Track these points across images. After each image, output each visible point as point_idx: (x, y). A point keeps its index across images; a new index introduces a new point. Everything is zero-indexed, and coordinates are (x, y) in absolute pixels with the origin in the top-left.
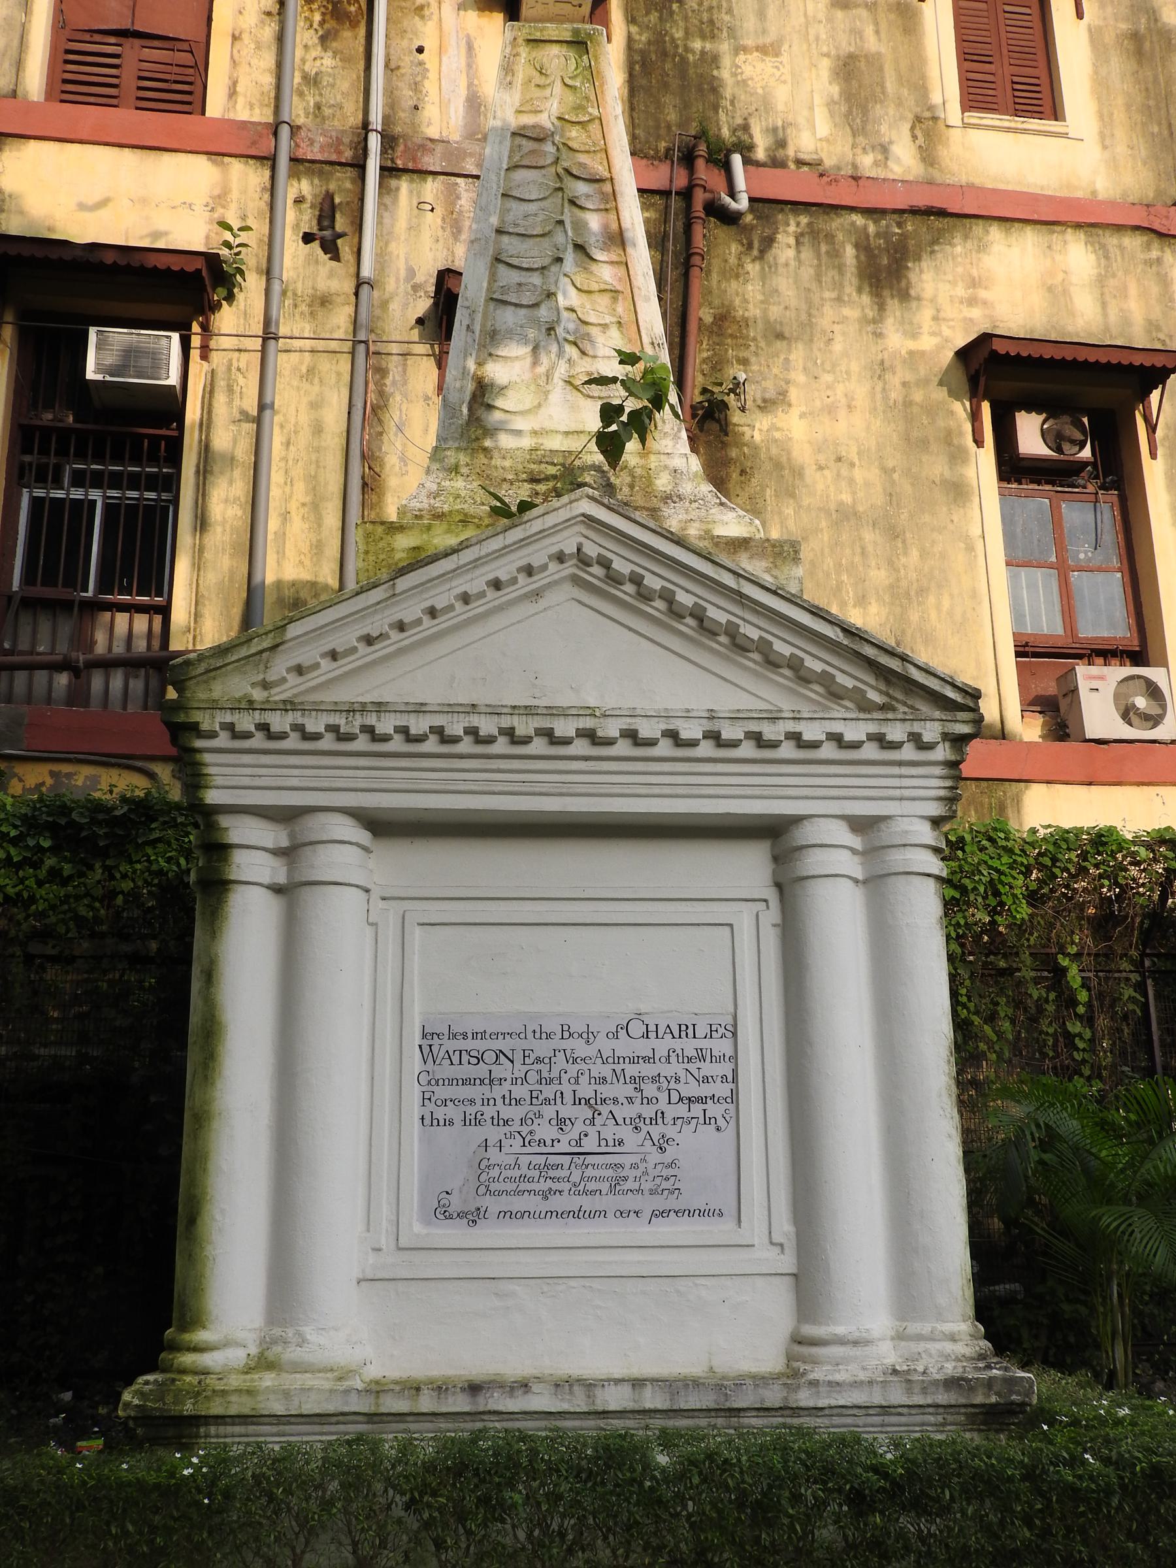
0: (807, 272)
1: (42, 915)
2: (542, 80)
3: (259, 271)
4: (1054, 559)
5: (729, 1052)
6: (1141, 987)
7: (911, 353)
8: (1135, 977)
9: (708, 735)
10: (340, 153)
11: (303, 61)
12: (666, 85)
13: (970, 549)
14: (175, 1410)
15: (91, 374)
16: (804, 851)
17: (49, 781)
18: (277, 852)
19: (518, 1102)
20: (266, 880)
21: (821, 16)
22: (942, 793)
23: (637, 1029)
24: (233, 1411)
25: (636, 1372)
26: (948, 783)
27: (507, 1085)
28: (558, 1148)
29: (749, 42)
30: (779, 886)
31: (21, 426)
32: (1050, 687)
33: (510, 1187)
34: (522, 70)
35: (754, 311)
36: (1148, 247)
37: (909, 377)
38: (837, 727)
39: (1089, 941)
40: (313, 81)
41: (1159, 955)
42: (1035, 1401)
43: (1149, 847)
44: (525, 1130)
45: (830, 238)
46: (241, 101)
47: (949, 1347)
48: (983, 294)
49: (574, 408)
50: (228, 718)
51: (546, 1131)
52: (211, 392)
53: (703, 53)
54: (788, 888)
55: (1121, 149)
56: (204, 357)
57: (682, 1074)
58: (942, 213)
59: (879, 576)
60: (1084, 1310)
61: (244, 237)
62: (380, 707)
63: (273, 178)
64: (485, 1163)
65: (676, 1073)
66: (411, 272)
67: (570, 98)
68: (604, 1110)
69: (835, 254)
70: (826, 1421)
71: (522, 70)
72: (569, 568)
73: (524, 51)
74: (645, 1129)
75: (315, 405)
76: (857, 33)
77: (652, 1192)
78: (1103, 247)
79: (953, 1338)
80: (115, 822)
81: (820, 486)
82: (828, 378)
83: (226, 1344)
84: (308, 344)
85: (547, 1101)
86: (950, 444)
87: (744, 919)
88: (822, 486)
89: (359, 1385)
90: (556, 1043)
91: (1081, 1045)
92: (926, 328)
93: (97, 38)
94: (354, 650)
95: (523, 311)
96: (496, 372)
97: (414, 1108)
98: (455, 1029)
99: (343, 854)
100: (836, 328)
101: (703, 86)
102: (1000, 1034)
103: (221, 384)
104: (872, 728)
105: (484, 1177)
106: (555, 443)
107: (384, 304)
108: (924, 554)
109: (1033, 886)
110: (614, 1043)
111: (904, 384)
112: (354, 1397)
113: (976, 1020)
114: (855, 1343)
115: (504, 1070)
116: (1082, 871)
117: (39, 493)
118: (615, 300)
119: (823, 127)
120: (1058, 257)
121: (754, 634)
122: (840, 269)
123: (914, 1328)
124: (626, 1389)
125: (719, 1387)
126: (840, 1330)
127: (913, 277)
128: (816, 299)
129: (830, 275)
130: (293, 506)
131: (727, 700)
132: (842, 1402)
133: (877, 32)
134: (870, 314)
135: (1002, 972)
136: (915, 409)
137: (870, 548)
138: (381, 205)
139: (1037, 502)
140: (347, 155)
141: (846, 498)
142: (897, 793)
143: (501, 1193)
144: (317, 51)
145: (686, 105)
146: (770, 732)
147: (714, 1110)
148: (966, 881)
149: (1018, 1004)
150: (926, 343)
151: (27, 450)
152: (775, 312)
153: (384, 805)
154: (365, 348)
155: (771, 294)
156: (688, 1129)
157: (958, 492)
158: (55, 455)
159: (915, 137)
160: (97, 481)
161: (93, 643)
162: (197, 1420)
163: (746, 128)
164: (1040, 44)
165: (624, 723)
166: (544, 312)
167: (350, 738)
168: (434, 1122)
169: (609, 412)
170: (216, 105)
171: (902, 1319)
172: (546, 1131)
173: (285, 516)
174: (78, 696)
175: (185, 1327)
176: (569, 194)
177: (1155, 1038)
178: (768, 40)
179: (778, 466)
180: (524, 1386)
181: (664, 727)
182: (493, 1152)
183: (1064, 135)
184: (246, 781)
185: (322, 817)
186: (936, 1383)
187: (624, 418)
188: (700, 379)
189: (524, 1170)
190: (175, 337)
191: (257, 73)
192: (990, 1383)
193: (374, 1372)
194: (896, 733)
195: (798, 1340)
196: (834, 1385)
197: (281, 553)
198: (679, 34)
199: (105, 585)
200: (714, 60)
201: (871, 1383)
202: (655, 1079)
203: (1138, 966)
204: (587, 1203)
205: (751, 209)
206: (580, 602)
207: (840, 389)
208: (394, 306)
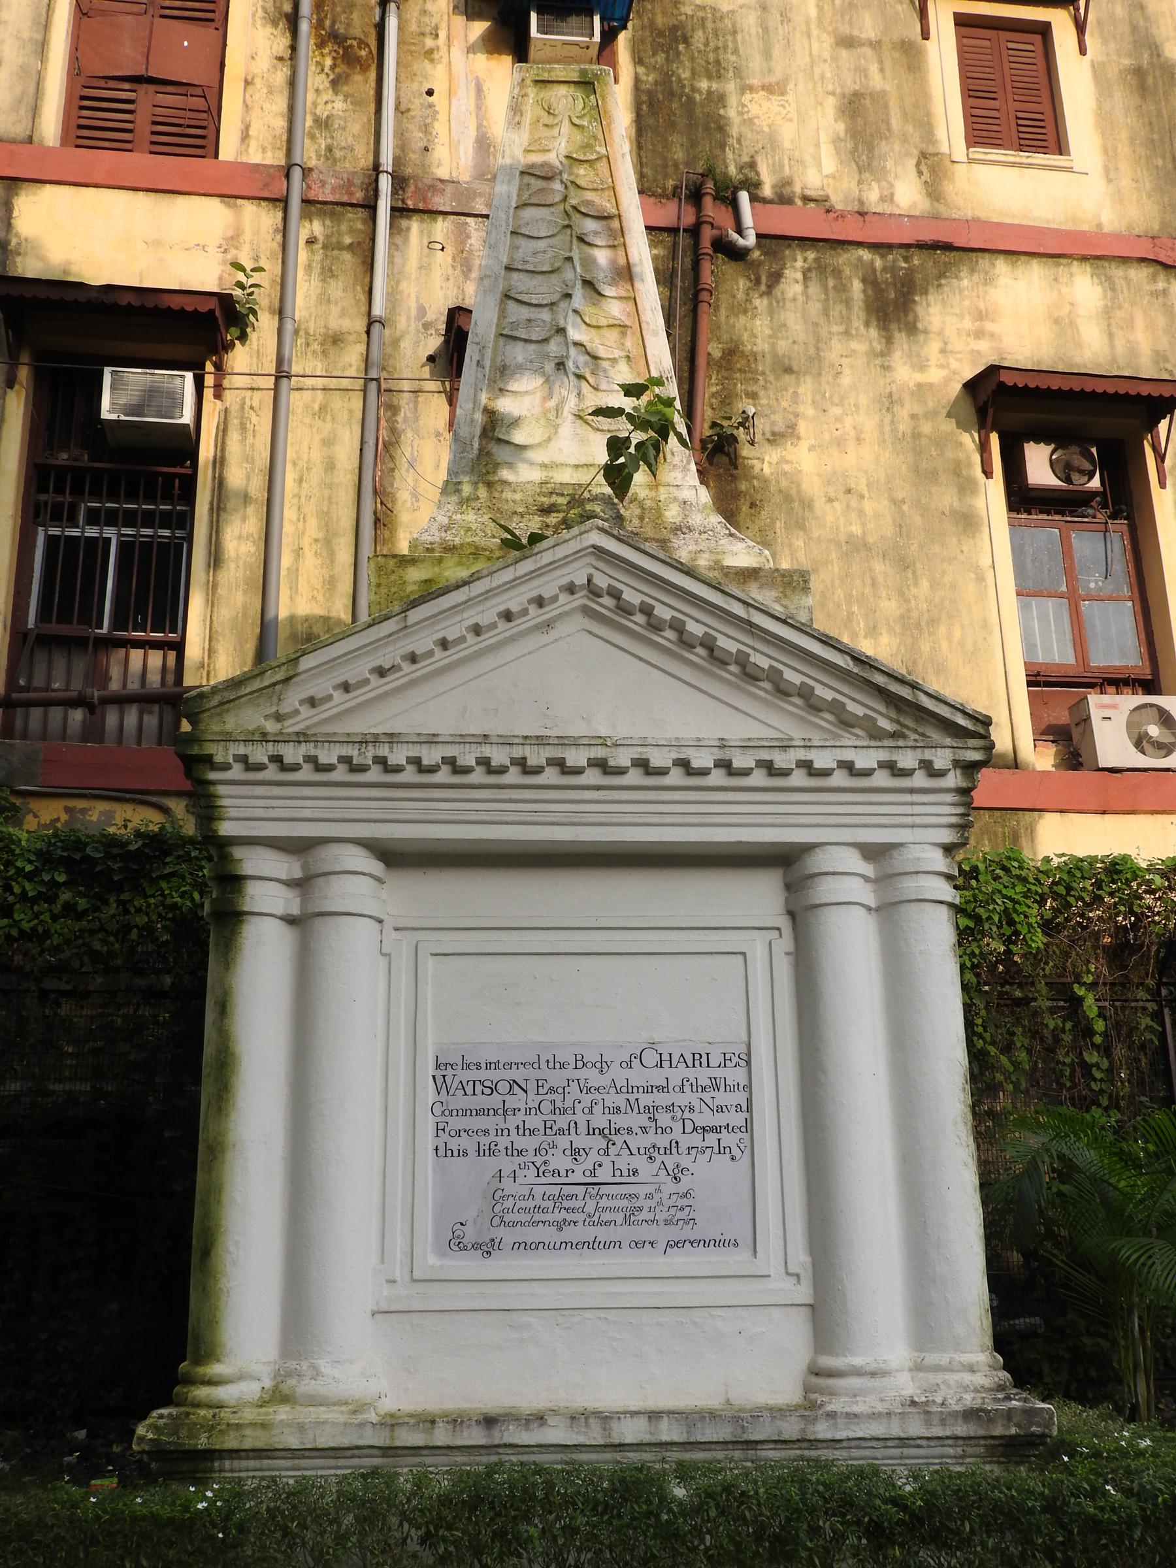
0: (815, 307)
2: (549, 120)
3: (271, 311)
4: (1064, 589)
6: (1158, 1016)
7: (919, 385)
8: (1152, 1006)
10: (351, 194)
11: (315, 105)
12: (673, 125)
13: (980, 579)
14: (189, 1444)
17: (64, 817)
18: (290, 884)
20: (280, 911)
21: (826, 55)
22: (954, 820)
23: (650, 1058)
24: (247, 1445)
25: (652, 1404)
27: (520, 1116)
29: (755, 82)
30: (791, 914)
31: (36, 465)
32: (1061, 716)
33: (527, 1217)
34: (530, 110)
35: (762, 346)
36: (1154, 278)
37: (918, 409)
38: (848, 755)
40: (323, 124)
44: (539, 1160)
45: (837, 272)
46: (253, 144)
47: (967, 1378)
48: (989, 326)
49: (583, 441)
51: (560, 1162)
52: (225, 431)
53: (710, 92)
54: (801, 915)
55: (1126, 183)
56: (218, 396)
57: (696, 1103)
58: (948, 247)
59: (889, 606)
61: (256, 278)
62: (392, 739)
63: (285, 219)
64: (499, 1194)
65: (691, 1106)
66: (422, 311)
67: (578, 137)
68: (619, 1139)
69: (842, 289)
70: (845, 1453)
71: (530, 110)
72: (580, 599)
73: (532, 92)
74: (659, 1159)
77: (667, 1223)
78: (1109, 279)
79: (971, 1369)
80: (129, 856)
81: (830, 519)
82: (837, 411)
84: (320, 382)
85: (561, 1131)
88: (831, 517)
89: (374, 1418)
91: (1098, 1075)
93: (112, 84)
94: (366, 682)
95: (533, 347)
98: (468, 1059)
99: (356, 885)
100: (845, 361)
101: (709, 124)
102: (1016, 1065)
103: (234, 422)
104: (884, 755)
105: (498, 1208)
106: (566, 476)
107: (395, 343)
108: (934, 585)
109: (1048, 915)
110: (627, 1073)
111: (913, 417)
112: (368, 1430)
113: (992, 1050)
114: (873, 1374)
115: (517, 1100)
116: (1098, 899)
117: (55, 531)
118: (624, 334)
119: (829, 164)
120: (1065, 290)
121: (764, 663)
122: (848, 303)
123: (932, 1358)
124: (642, 1423)
125: (736, 1419)
126: (857, 1361)
127: (920, 310)
128: (824, 332)
129: (838, 309)
130: (306, 542)
132: (860, 1434)
133: (882, 70)
134: (878, 347)
135: (1018, 1002)
136: (924, 441)
138: (393, 245)
139: (1046, 532)
140: (359, 196)
141: (856, 529)
142: (909, 820)
143: (515, 1224)
144: (328, 95)
145: (693, 144)
147: (728, 1139)
148: (980, 911)
149: (1035, 1034)
150: (934, 375)
152: (783, 346)
154: (376, 386)
157: (968, 522)
159: (920, 173)
160: (111, 519)
163: (752, 165)
165: (635, 753)
167: (363, 769)
168: (448, 1152)
169: (616, 445)
170: (229, 148)
172: (560, 1162)
173: (298, 552)
174: (93, 732)
176: (577, 231)
178: (773, 80)
179: (788, 498)
180: (540, 1418)
181: (675, 756)
182: (507, 1183)
183: (1069, 170)
185: (335, 849)
188: (709, 413)
189: (538, 1201)
190: (189, 376)
191: (270, 116)
193: (388, 1405)
194: (907, 760)
195: (816, 1372)
196: (853, 1417)
197: (294, 588)
198: (685, 75)
199: (119, 621)
200: (721, 99)
201: (889, 1414)
202: (670, 1108)
203: (1155, 995)
204: (603, 1234)
205: (759, 245)
206: (590, 633)
207: (849, 421)
208: (406, 345)
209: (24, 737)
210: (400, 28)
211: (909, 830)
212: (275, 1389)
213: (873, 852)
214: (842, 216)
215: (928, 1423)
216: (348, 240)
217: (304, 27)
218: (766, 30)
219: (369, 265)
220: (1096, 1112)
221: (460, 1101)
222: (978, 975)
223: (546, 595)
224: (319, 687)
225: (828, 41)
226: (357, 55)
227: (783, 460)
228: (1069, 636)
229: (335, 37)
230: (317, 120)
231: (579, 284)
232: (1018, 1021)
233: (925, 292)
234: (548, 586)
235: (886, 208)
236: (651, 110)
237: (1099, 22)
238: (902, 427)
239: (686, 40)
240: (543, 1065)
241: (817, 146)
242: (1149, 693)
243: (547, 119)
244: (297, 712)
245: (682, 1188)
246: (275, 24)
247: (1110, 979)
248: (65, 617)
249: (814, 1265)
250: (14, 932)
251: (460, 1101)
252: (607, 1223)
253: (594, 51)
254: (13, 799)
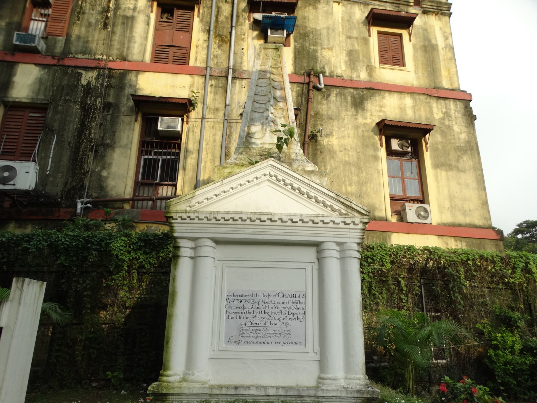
0: (338, 103)
1: (142, 262)
2: (267, 58)
3: (201, 103)
5: (304, 302)
6: (420, 287)
7: (364, 123)
8: (418, 284)
9: (300, 220)
10: (222, 74)
11: (214, 52)
12: (304, 57)
13: (379, 172)
14: (161, 392)
15: (159, 128)
17: (146, 228)
18: (192, 248)
19: (250, 313)
20: (189, 256)
21: (344, 40)
22: (360, 237)
24: (175, 392)
25: (278, 384)
26: (362, 234)
27: (247, 309)
28: (260, 325)
29: (325, 47)
30: (318, 259)
32: (399, 208)
33: (248, 335)
34: (262, 55)
35: (324, 112)
36: (426, 99)
37: (364, 129)
38: (333, 219)
39: (406, 275)
40: (216, 57)
41: (425, 279)
42: (380, 397)
43: (422, 251)
44: (252, 320)
45: (344, 95)
46: (198, 62)
47: (358, 382)
48: (383, 109)
49: (272, 137)
50: (180, 215)
51: (257, 321)
52: (189, 132)
53: (313, 49)
54: (320, 259)
55: (420, 74)
56: (187, 123)
57: (292, 307)
58: (373, 89)
59: (355, 179)
60: (403, 372)
61: (197, 95)
62: (218, 212)
63: (205, 80)
65: (289, 307)
66: (239, 103)
67: (274, 62)
68: (272, 316)
69: (346, 99)
70: (326, 400)
71: (262, 55)
72: (268, 177)
73: (263, 51)
74: (282, 321)
75: (214, 135)
76: (353, 45)
77: (283, 337)
78: (415, 98)
79: (359, 379)
80: (160, 239)
81: (340, 156)
82: (343, 129)
83: (175, 375)
84: (213, 120)
85: (257, 313)
86: (374, 146)
87: (309, 267)
88: (341, 155)
89: (207, 386)
90: (260, 298)
91: (404, 301)
92: (368, 117)
93: (163, 47)
94: (212, 198)
95: (260, 114)
96: (253, 129)
97: (224, 314)
98: (235, 294)
99: (208, 249)
100: (346, 117)
101: (313, 57)
102: (383, 298)
103: (191, 130)
104: (342, 220)
106: (267, 146)
107: (232, 110)
108: (367, 174)
109: (392, 259)
110: (275, 298)
111: (363, 131)
112: (206, 389)
113: (377, 293)
114: (334, 379)
115: (247, 305)
116: (405, 257)
117: (146, 157)
118: (283, 111)
119: (343, 67)
120: (403, 101)
122: (347, 102)
123: (349, 376)
124: (274, 389)
125: (298, 390)
126: (330, 376)
127: (365, 105)
128: (341, 110)
129: (344, 104)
130: (208, 160)
132: (330, 395)
133: (358, 45)
134: (354, 114)
135: (384, 281)
136: (365, 137)
137: (353, 172)
138: (232, 86)
139: (397, 161)
140: (224, 74)
141: (347, 159)
142: (348, 236)
143: (245, 337)
144: (217, 50)
145: (309, 62)
146: (316, 220)
147: (300, 316)
148: (374, 258)
149: (388, 290)
150: (369, 121)
151: (143, 146)
152: (330, 113)
153: (219, 236)
154: (227, 121)
155: (329, 108)
156: (293, 321)
157: (376, 158)
159: (367, 70)
160: (160, 154)
161: (158, 194)
162: (167, 395)
163: (324, 68)
164: (400, 48)
165: (279, 217)
166: (265, 114)
167: (210, 220)
168: (229, 318)
169: (279, 139)
170: (192, 63)
171: (347, 374)
172: (257, 321)
173: (206, 162)
174: (154, 207)
175: (165, 371)
176: (273, 85)
177: (424, 301)
178: (330, 46)
179: (330, 151)
180: (249, 387)
181: (289, 218)
182: (244, 326)
183: (405, 71)
184: (184, 231)
185: (203, 240)
186: (354, 391)
187: (283, 141)
188: (310, 129)
189: (251, 331)
190: (180, 119)
191: (202, 55)
192: (368, 392)
193: (212, 383)
194: (348, 221)
195: (320, 378)
196: (328, 390)
197: (204, 171)
198: (307, 45)
199: (161, 179)
200: (316, 51)
201: (337, 390)
202: (285, 308)
203: (419, 281)
204: (267, 340)
205: (325, 87)
207: (346, 132)
208: (234, 111)
209: (137, 208)
210: (236, 33)
212: (183, 378)
213: (339, 244)
214: (346, 80)
215: (347, 393)
216: (221, 85)
217: (211, 33)
218: (328, 34)
219: (226, 91)
220: (403, 311)
221: (232, 305)
222: (374, 274)
223: (258, 177)
224: (200, 199)
225: (344, 37)
226: (224, 40)
227: (329, 141)
228: (401, 188)
229: (219, 35)
230: (214, 56)
231: (272, 98)
232: (384, 286)
233: (367, 100)
234: (258, 174)
235: (358, 79)
236: (298, 55)
237: (415, 34)
238: (360, 134)
239: (308, 36)
241: (341, 63)
243: (266, 57)
244: (195, 205)
245: (288, 329)
246: (204, 32)
247: (408, 277)
249: (320, 350)
250: (131, 258)
251: (232, 305)
252: (268, 337)
253: (284, 39)
254: (133, 224)
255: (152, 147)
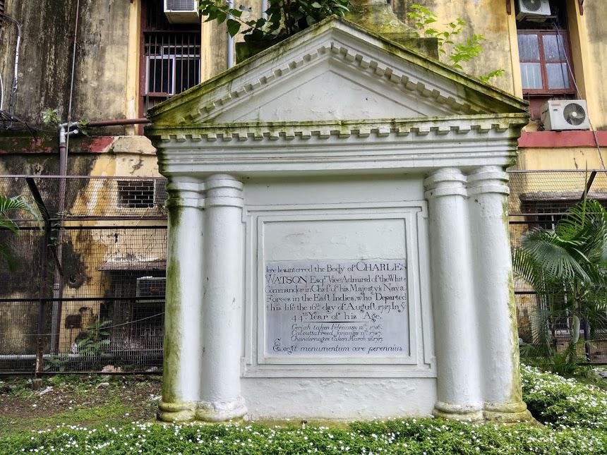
4: (539, 59)
15: (166, 10)
16: (440, 199)
18: (200, 193)
22: (508, 154)
23: (361, 267)
30: (427, 200)
31: (144, 33)
38: (455, 124)
44: (312, 311)
64: (295, 326)
65: (382, 286)
68: (347, 302)
74: (366, 311)
87: (410, 216)
90: (325, 273)
99: (229, 193)
105: (294, 333)
117: (152, 57)
121: (415, 81)
126: (458, 406)
131: (401, 114)
158: (157, 42)
160: (172, 52)
189: (312, 330)
199: (178, 91)
206: (333, 72)
211: (486, 159)
213: (467, 171)
240: (314, 270)
242: (572, 99)
245: (376, 324)
248: (158, 90)
255: (159, 42)
